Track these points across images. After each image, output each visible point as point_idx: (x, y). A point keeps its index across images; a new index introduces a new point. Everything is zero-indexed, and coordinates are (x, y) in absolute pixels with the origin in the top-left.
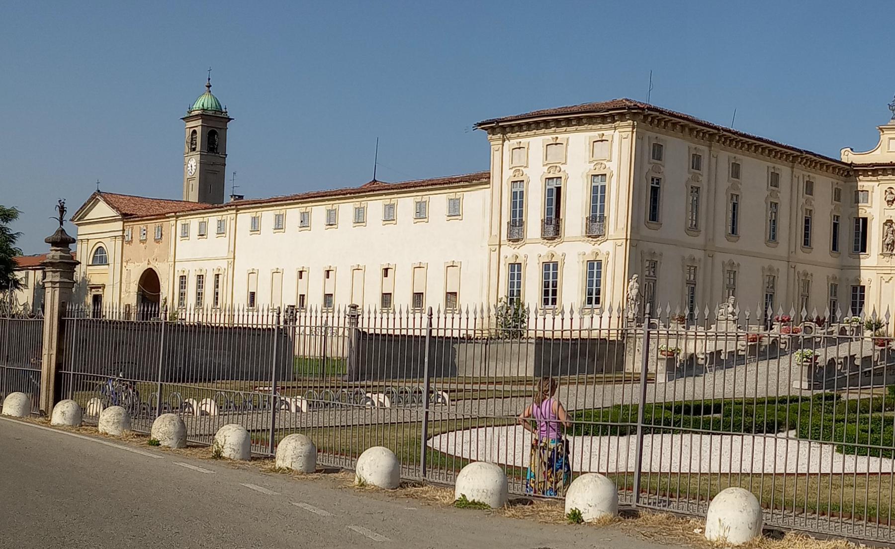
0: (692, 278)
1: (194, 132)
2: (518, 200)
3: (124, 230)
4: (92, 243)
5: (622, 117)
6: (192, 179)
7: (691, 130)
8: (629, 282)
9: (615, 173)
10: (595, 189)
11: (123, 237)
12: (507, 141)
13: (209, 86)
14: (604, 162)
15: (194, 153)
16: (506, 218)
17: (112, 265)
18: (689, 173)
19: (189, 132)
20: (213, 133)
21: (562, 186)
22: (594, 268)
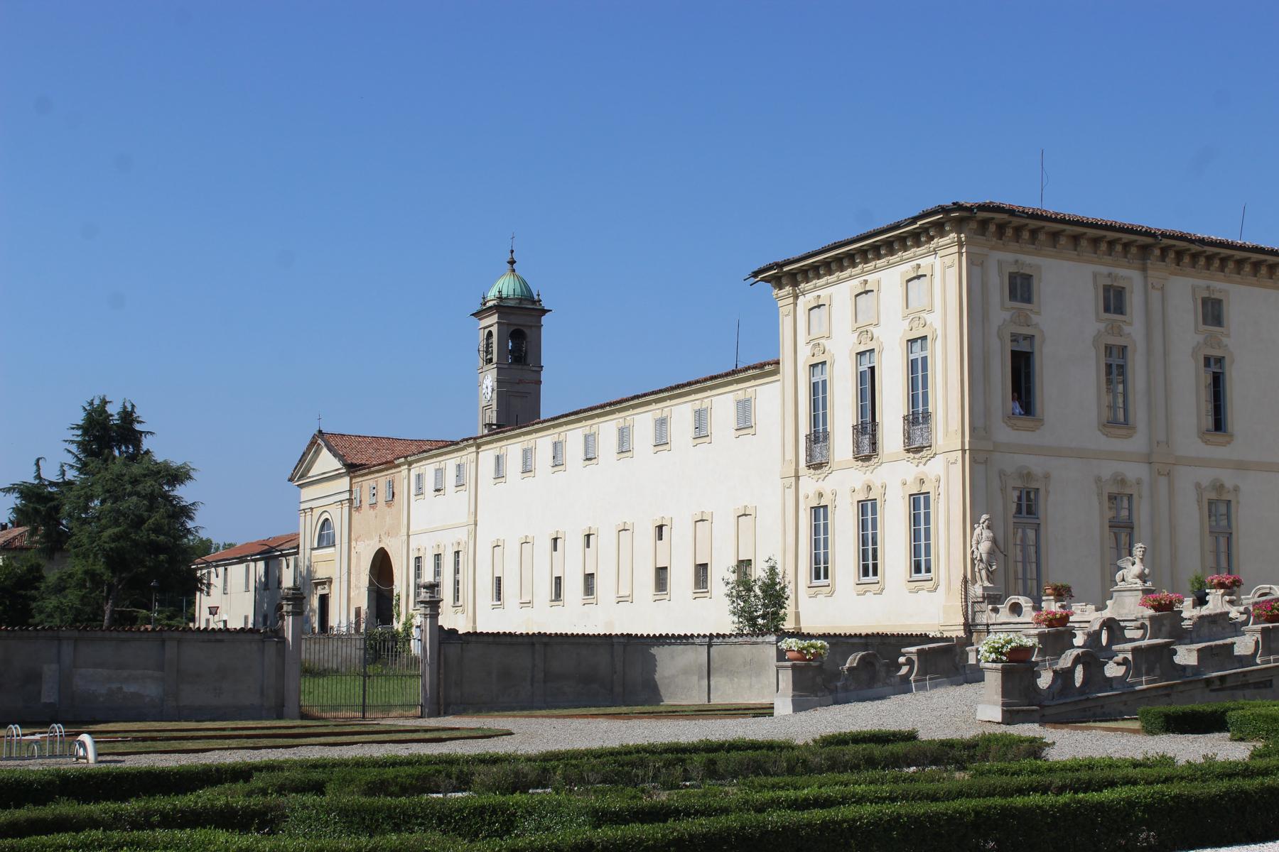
0: (1125, 513)
1: (490, 334)
2: (818, 393)
3: (351, 491)
4: (317, 512)
5: (940, 228)
6: (488, 407)
7: (1095, 242)
8: (973, 529)
9: (939, 333)
10: (913, 365)
11: (350, 500)
12: (801, 298)
13: (512, 262)
14: (923, 315)
15: (490, 366)
16: (804, 429)
17: (338, 546)
18: (1098, 319)
19: (482, 335)
20: (518, 332)
21: (876, 365)
22: (919, 504)
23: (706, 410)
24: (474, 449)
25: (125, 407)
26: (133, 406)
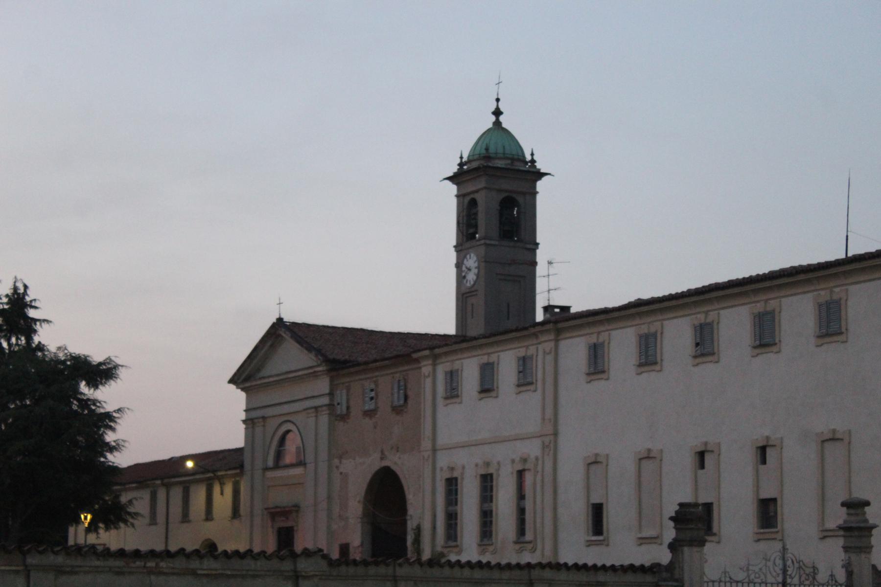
3: (331, 394)
4: (272, 424)
17: (311, 467)
23: (603, 344)
24: (552, 337)
25: (15, 289)
26: (26, 287)
